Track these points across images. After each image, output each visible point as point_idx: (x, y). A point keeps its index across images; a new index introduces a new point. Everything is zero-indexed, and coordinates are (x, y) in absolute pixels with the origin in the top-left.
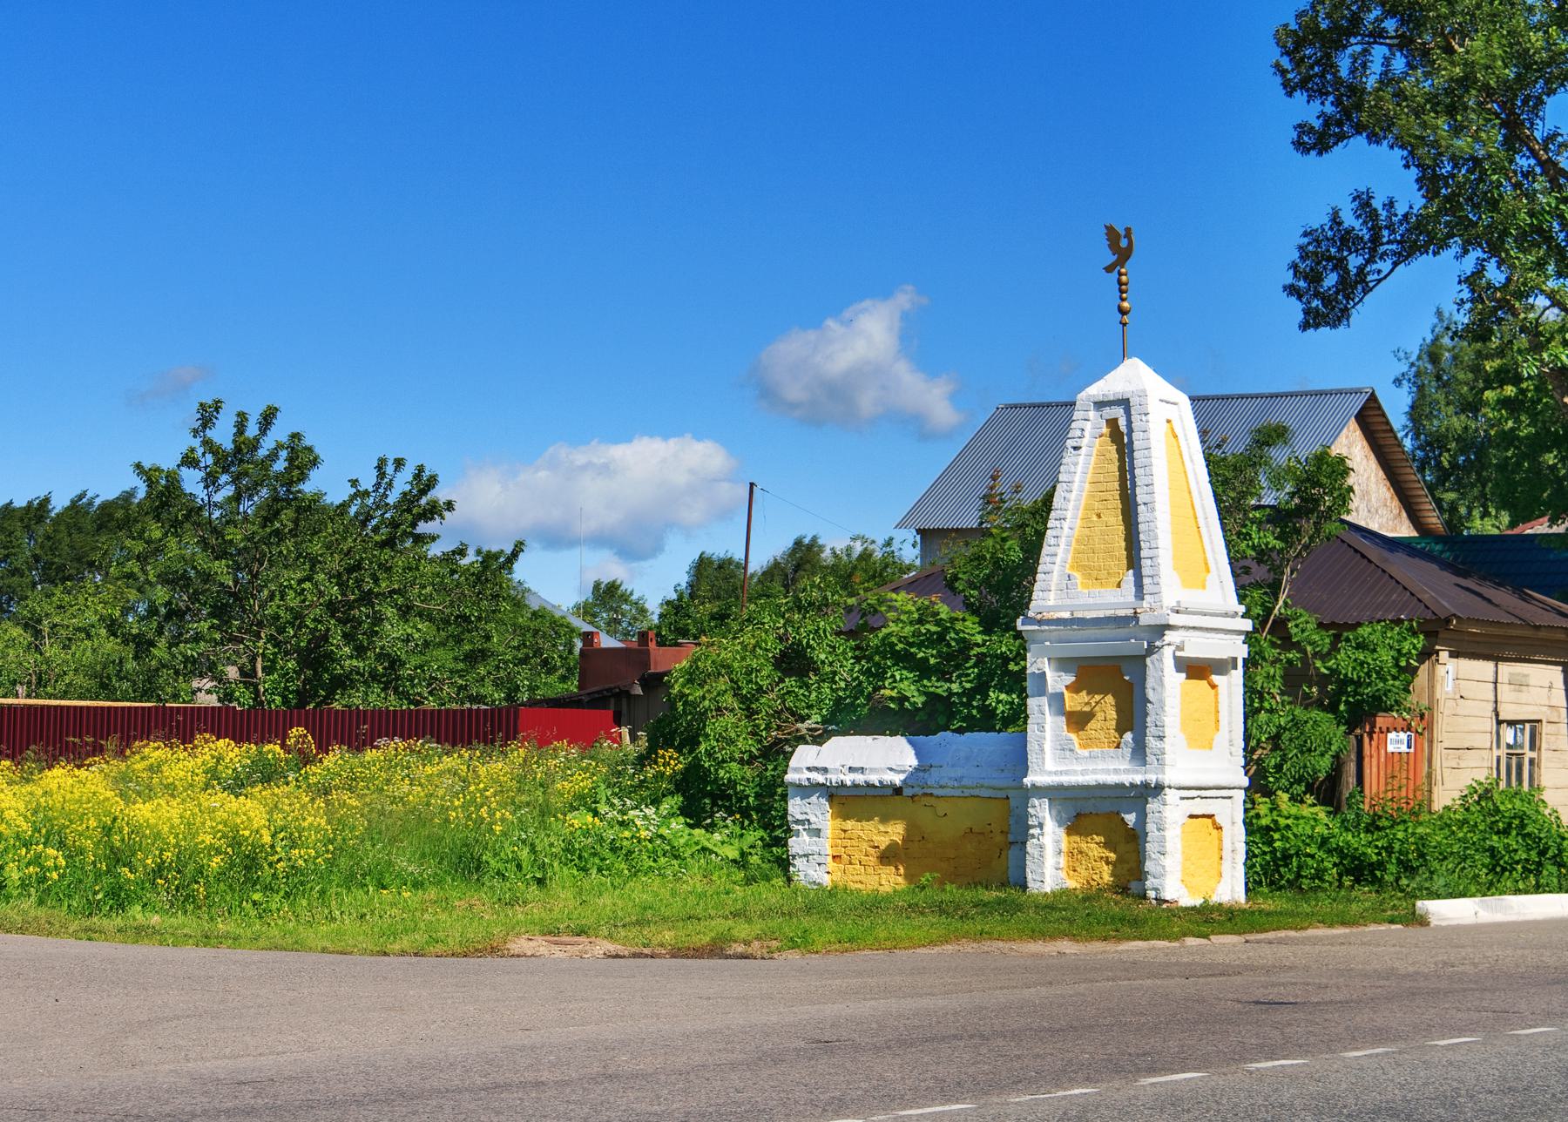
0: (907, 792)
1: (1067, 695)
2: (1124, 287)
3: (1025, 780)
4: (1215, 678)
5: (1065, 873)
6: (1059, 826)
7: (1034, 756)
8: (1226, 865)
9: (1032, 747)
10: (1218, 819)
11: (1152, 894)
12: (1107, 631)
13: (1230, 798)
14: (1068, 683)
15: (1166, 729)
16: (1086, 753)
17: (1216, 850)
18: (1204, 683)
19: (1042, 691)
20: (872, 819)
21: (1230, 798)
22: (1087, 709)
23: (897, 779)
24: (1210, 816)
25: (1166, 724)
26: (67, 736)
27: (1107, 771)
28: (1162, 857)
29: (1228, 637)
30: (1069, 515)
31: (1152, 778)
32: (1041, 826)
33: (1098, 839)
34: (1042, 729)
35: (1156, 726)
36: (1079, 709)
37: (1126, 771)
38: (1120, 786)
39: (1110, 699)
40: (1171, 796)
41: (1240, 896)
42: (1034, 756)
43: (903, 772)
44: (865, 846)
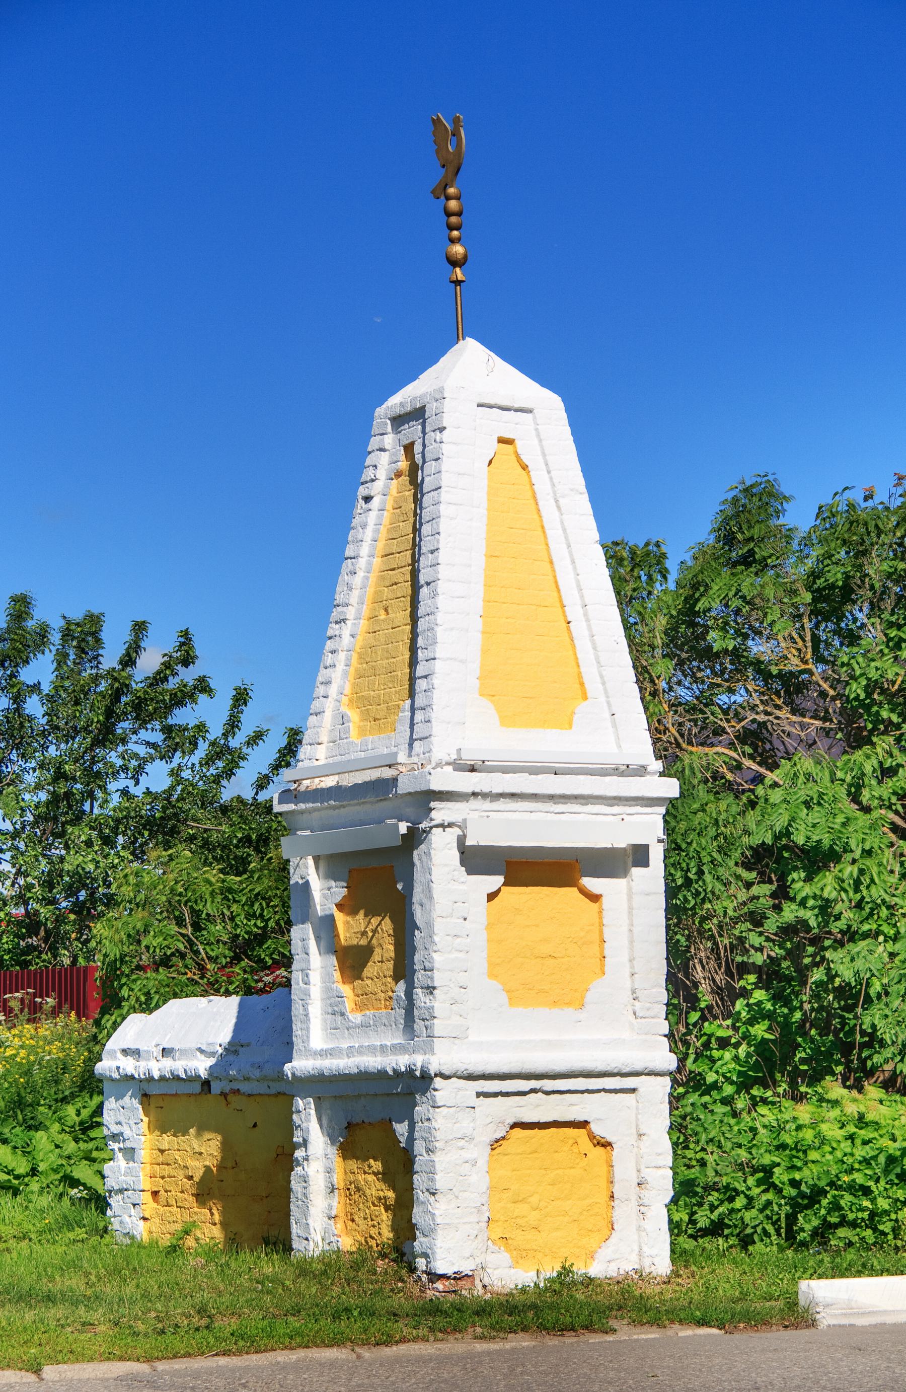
0: (216, 1087)
1: (340, 919)
2: (454, 220)
3: (288, 1068)
4: (591, 883)
5: (340, 1225)
6: (333, 1143)
7: (299, 1024)
8: (623, 1213)
9: (297, 1010)
10: (596, 1128)
11: (421, 1263)
12: (353, 810)
13: (633, 1090)
14: (338, 899)
15: (436, 974)
16: (356, 1018)
17: (603, 1183)
18: (571, 892)
19: (306, 916)
20: (185, 1133)
21: (633, 1090)
22: (363, 942)
23: (202, 1066)
24: (584, 1124)
25: (436, 965)
26: (5, 994)
27: (372, 1050)
28: (432, 1199)
29: (616, 809)
30: (350, 613)
31: (418, 1060)
32: (305, 1143)
33: (377, 1166)
34: (305, 972)
35: (425, 970)
36: (355, 943)
37: (397, 1049)
38: (381, 1074)
39: (387, 920)
40: (444, 1091)
41: (662, 1265)
42: (299, 1024)
43: (213, 1054)
44: (180, 1174)
